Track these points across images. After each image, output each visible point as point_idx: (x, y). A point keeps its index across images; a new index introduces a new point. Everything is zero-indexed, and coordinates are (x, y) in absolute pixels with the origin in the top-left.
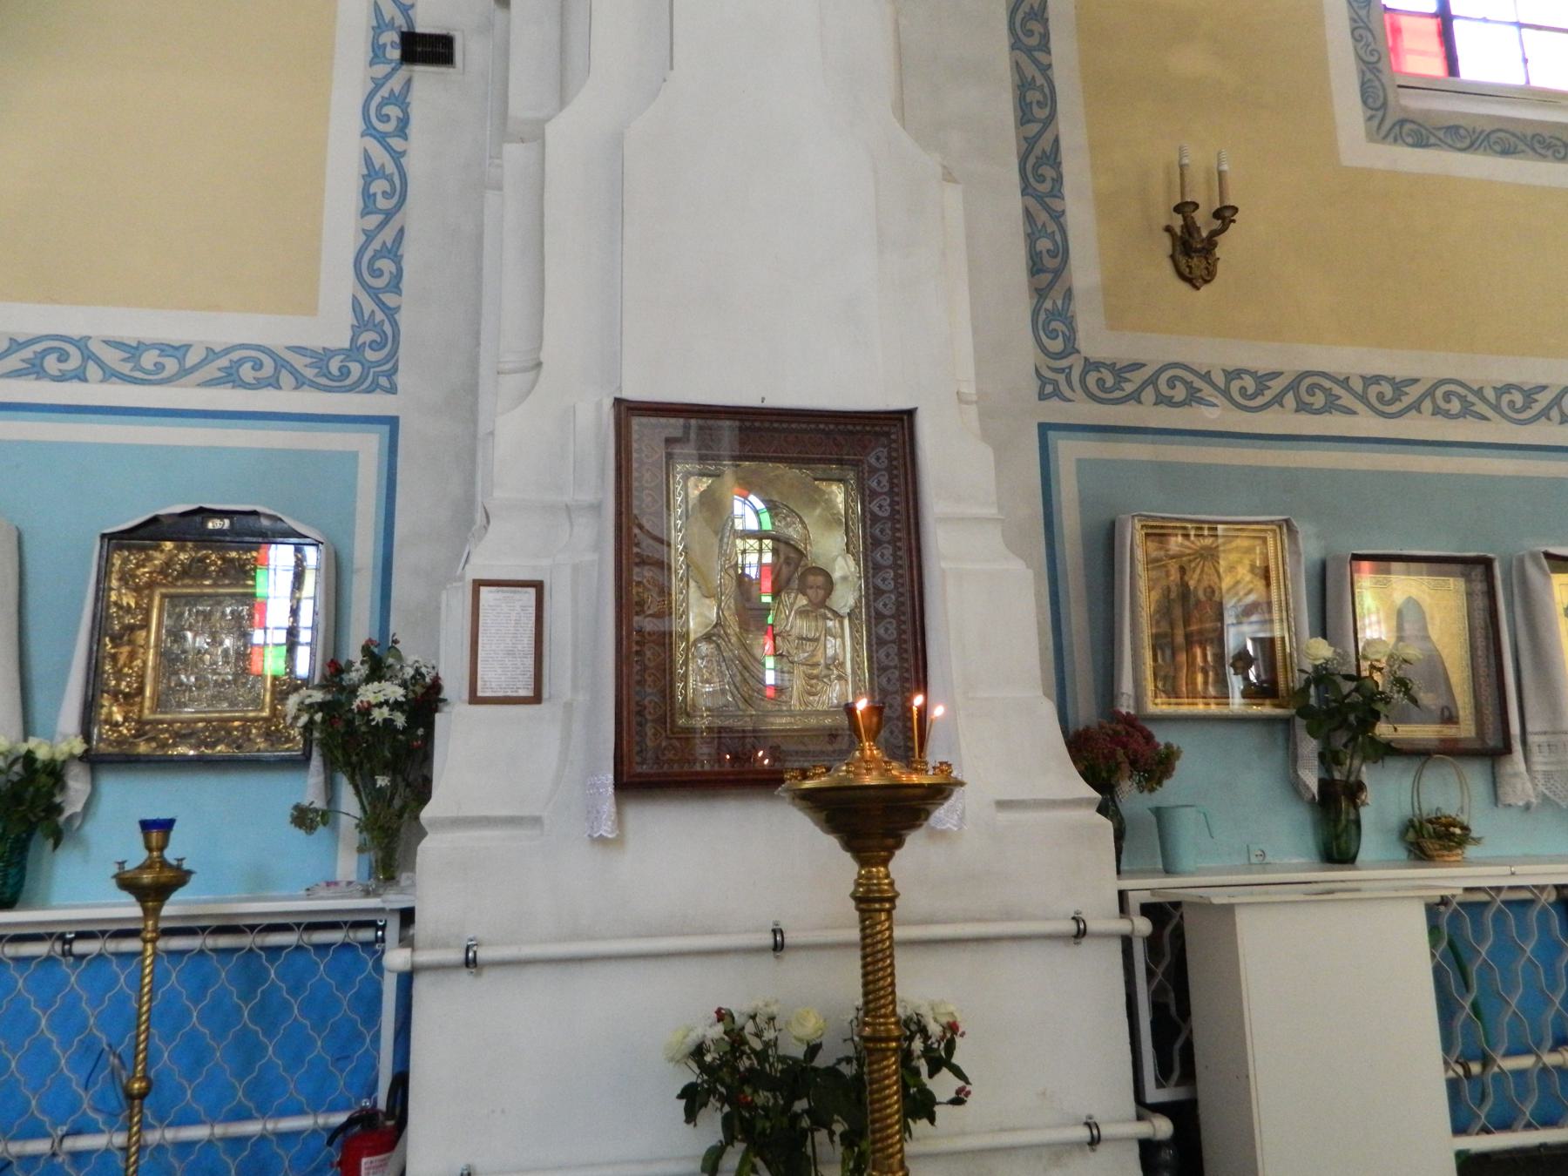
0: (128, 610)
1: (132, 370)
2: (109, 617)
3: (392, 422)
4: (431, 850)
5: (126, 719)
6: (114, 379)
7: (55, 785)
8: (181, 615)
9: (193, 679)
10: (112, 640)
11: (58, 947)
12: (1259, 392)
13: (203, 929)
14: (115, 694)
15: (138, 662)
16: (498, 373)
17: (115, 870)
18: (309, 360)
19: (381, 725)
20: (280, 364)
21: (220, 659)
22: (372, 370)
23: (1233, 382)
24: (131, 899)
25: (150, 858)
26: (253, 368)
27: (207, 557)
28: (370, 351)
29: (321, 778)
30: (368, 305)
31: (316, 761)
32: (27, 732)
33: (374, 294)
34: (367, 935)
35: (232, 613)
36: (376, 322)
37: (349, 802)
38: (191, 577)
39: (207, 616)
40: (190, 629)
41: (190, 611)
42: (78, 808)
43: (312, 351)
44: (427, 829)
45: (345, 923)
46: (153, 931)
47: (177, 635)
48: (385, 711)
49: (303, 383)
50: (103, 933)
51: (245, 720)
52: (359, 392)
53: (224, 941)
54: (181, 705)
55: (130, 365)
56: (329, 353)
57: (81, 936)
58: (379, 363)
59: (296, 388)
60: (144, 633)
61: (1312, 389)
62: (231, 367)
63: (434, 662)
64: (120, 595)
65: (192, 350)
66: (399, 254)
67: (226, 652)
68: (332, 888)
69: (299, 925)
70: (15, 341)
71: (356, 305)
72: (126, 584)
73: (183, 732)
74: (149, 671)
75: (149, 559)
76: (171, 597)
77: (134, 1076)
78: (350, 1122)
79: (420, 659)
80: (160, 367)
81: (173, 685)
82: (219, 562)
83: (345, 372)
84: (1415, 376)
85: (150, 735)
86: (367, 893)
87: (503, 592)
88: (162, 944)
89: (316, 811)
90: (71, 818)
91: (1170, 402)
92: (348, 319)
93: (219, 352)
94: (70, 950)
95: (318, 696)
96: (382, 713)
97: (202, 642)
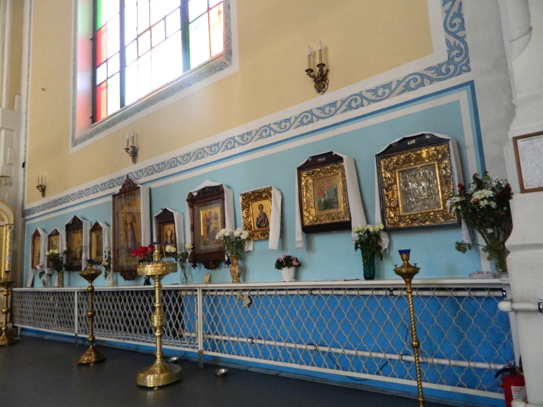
0: (389, 179)
1: (376, 97)
2: (383, 182)
3: (471, 83)
4: (511, 260)
5: (395, 216)
6: (371, 103)
7: (377, 239)
8: (406, 177)
9: (414, 199)
10: (386, 190)
11: (388, 293)
13: (433, 289)
14: (390, 208)
15: (395, 196)
16: (511, 42)
17: (394, 268)
18: (433, 71)
19: (485, 207)
20: (423, 76)
21: (422, 190)
22: (459, 66)
24: (401, 278)
25: (404, 263)
26: (414, 82)
27: (410, 155)
28: (457, 58)
29: (467, 231)
30: (452, 39)
31: (464, 225)
32: (368, 222)
33: (454, 35)
34: (499, 294)
35: (423, 173)
36: (457, 45)
37: (481, 242)
38: (407, 163)
39: (415, 176)
40: (410, 182)
41: (409, 175)
42: (386, 247)
43: (434, 67)
44: (510, 250)
45: (487, 289)
46: (410, 289)
47: (406, 185)
48: (486, 202)
49: (433, 81)
50: (400, 288)
51: (434, 212)
52: (455, 76)
53: (442, 293)
54: (412, 209)
56: (440, 65)
57: (396, 289)
58: (461, 61)
59: (430, 84)
60: (395, 186)
62: (406, 85)
63: (506, 178)
64: (385, 174)
65: (393, 84)
67: (423, 188)
68: (481, 274)
69: (468, 289)
70: (362, 106)
71: (448, 42)
72: (387, 170)
73: (414, 218)
74: (399, 199)
75: (392, 160)
76: (402, 172)
77: (413, 340)
78: (504, 370)
79: (499, 178)
80: (384, 93)
81: (408, 202)
82: (414, 156)
83: (448, 70)
84: (223, 152)
85: (403, 221)
86: (495, 277)
87: (529, 140)
88: (414, 293)
89: (465, 244)
90: (385, 250)
92: (445, 48)
94: (392, 294)
95: (458, 199)
96: (484, 203)
97: (414, 185)
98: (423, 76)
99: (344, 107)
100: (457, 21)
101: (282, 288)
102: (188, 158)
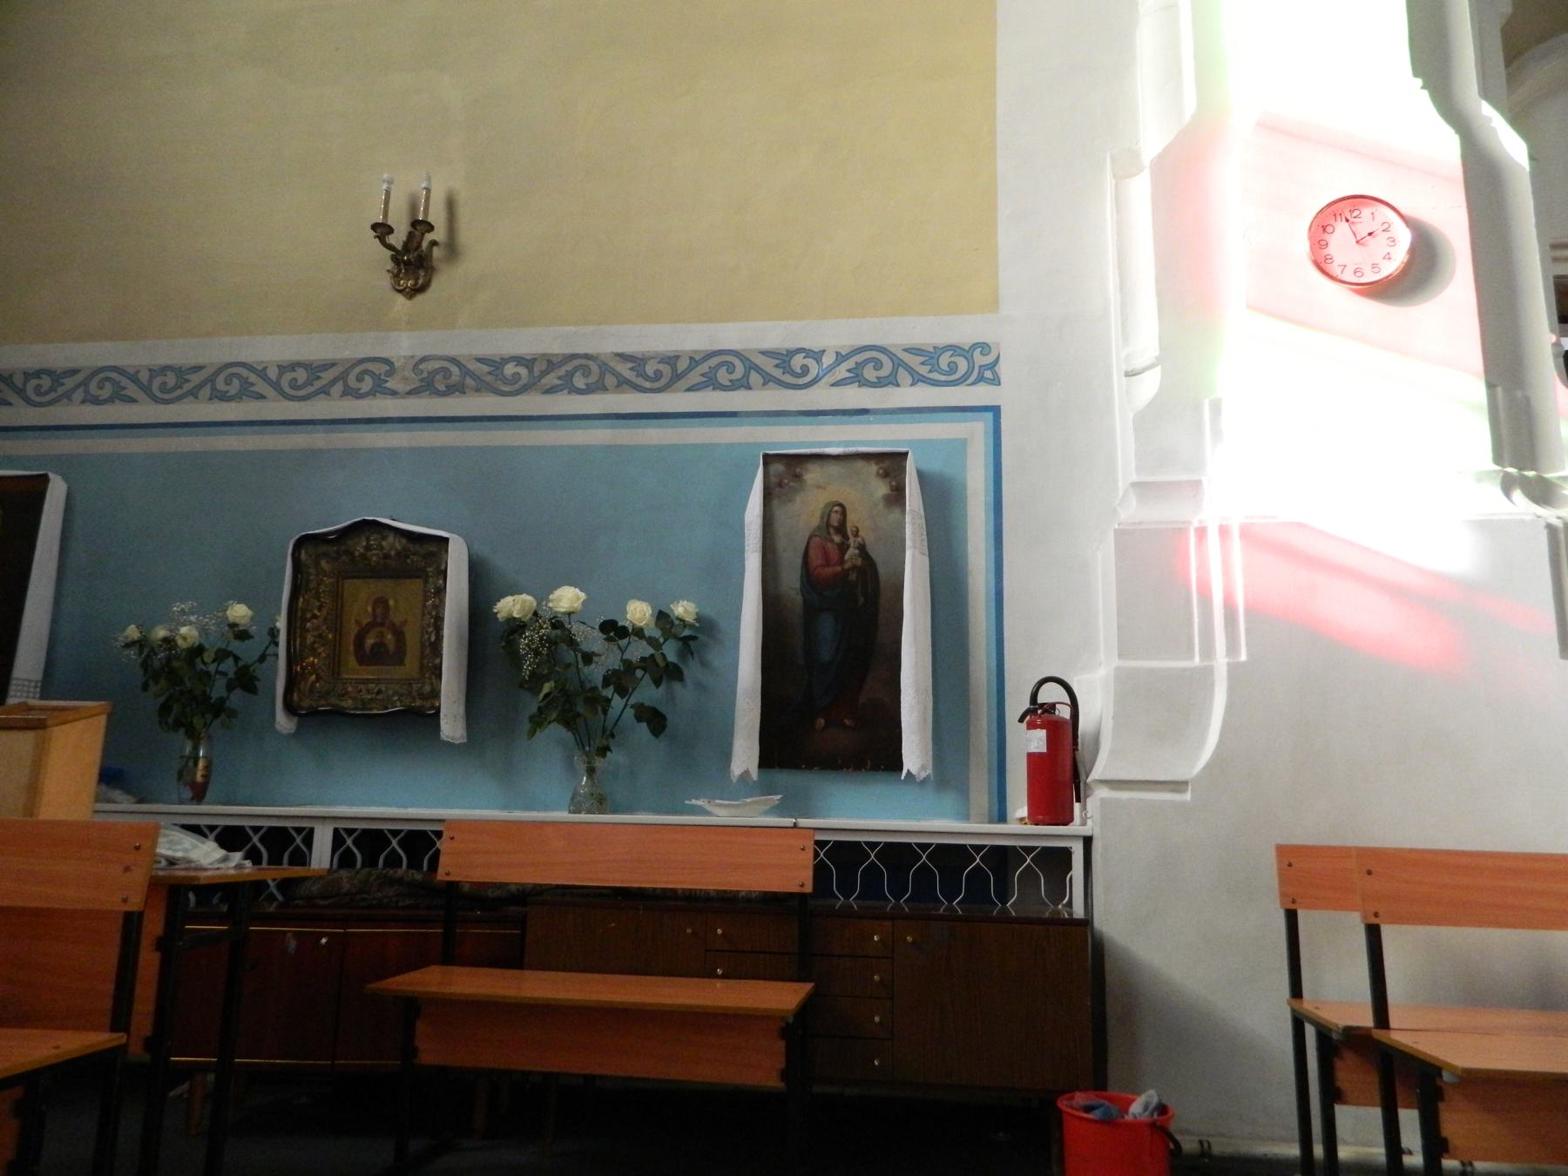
20: (605, 368)
23: (739, 376)
55: (928, 368)
61: (803, 372)
66: (377, 394)
84: (835, 389)
91: (97, 401)
93: (700, 360)
98: (896, 361)
100: (944, 360)
101: (1089, 896)
102: (220, 384)
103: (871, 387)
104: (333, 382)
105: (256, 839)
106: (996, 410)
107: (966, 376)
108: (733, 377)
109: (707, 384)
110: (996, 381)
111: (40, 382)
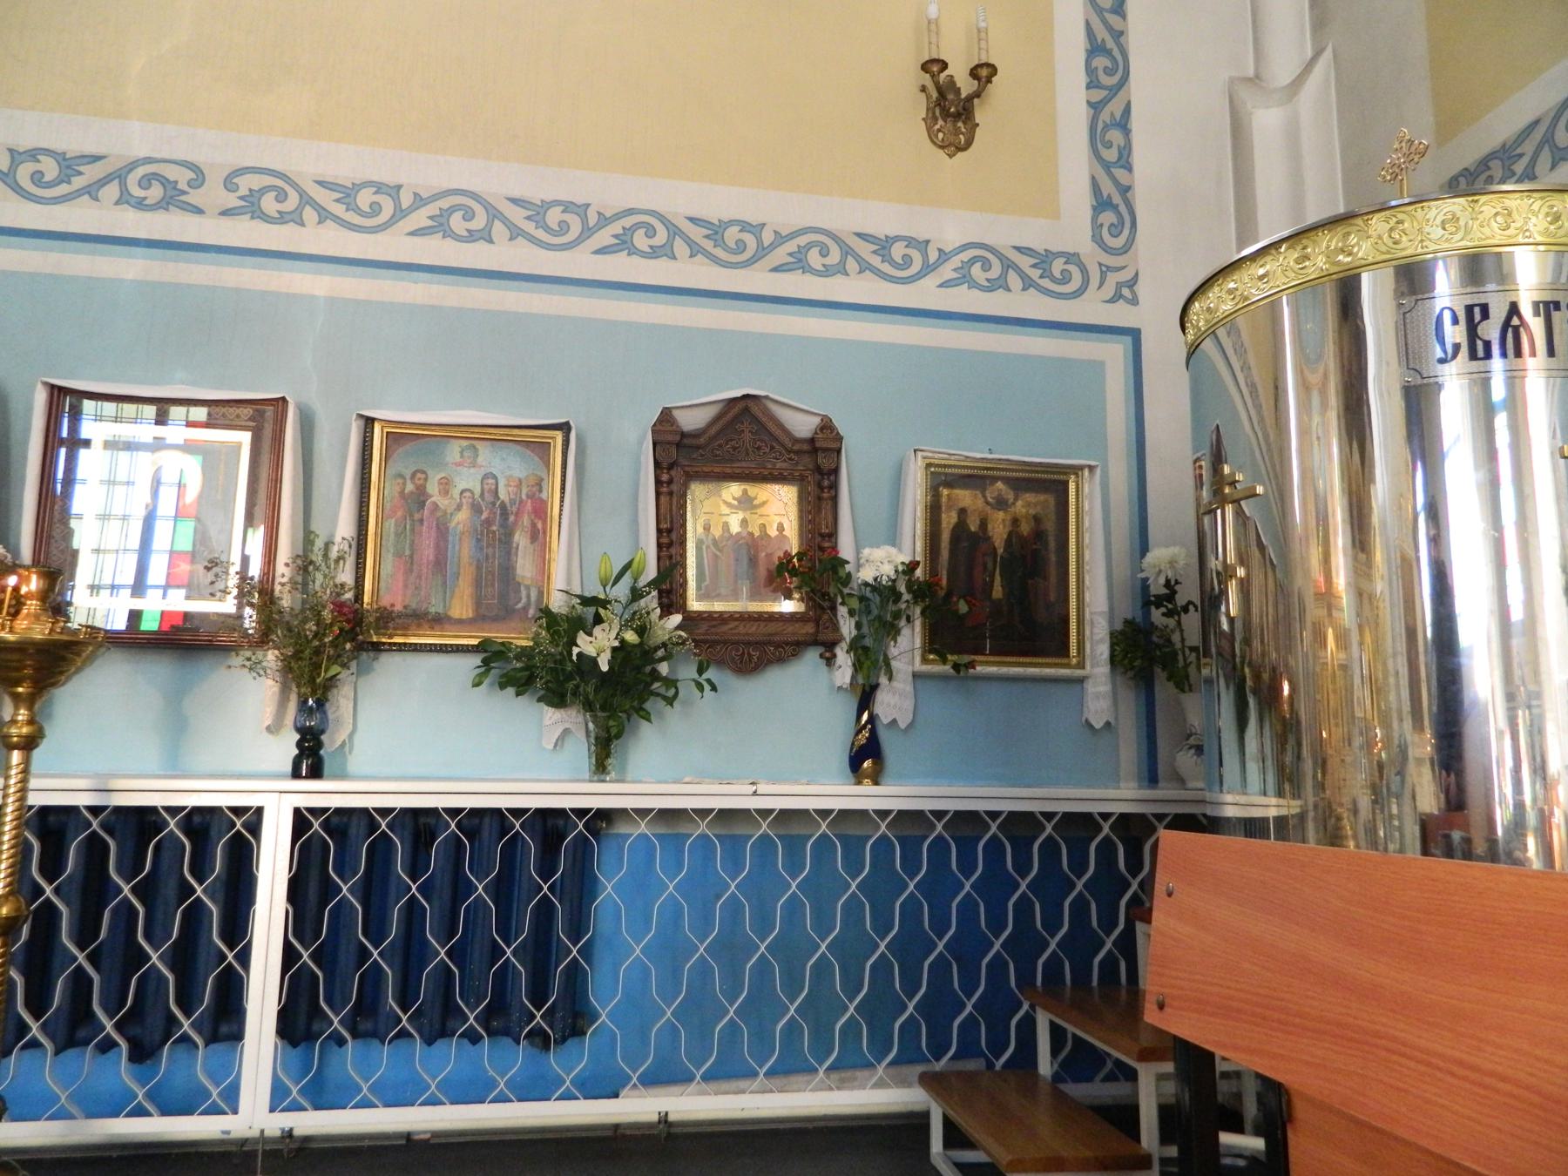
6: (1092, 111)
12: (803, 251)
20: (674, 231)
23: (481, 227)
62: (441, 215)
80: (1109, 145)
91: (140, 205)
99: (1107, 188)
103: (350, 229)
104: (104, 182)
105: (95, 825)
106: (1135, 334)
107: (23, 193)
108: (828, 261)
109: (959, 281)
110: (1134, 301)
111: (38, 167)
